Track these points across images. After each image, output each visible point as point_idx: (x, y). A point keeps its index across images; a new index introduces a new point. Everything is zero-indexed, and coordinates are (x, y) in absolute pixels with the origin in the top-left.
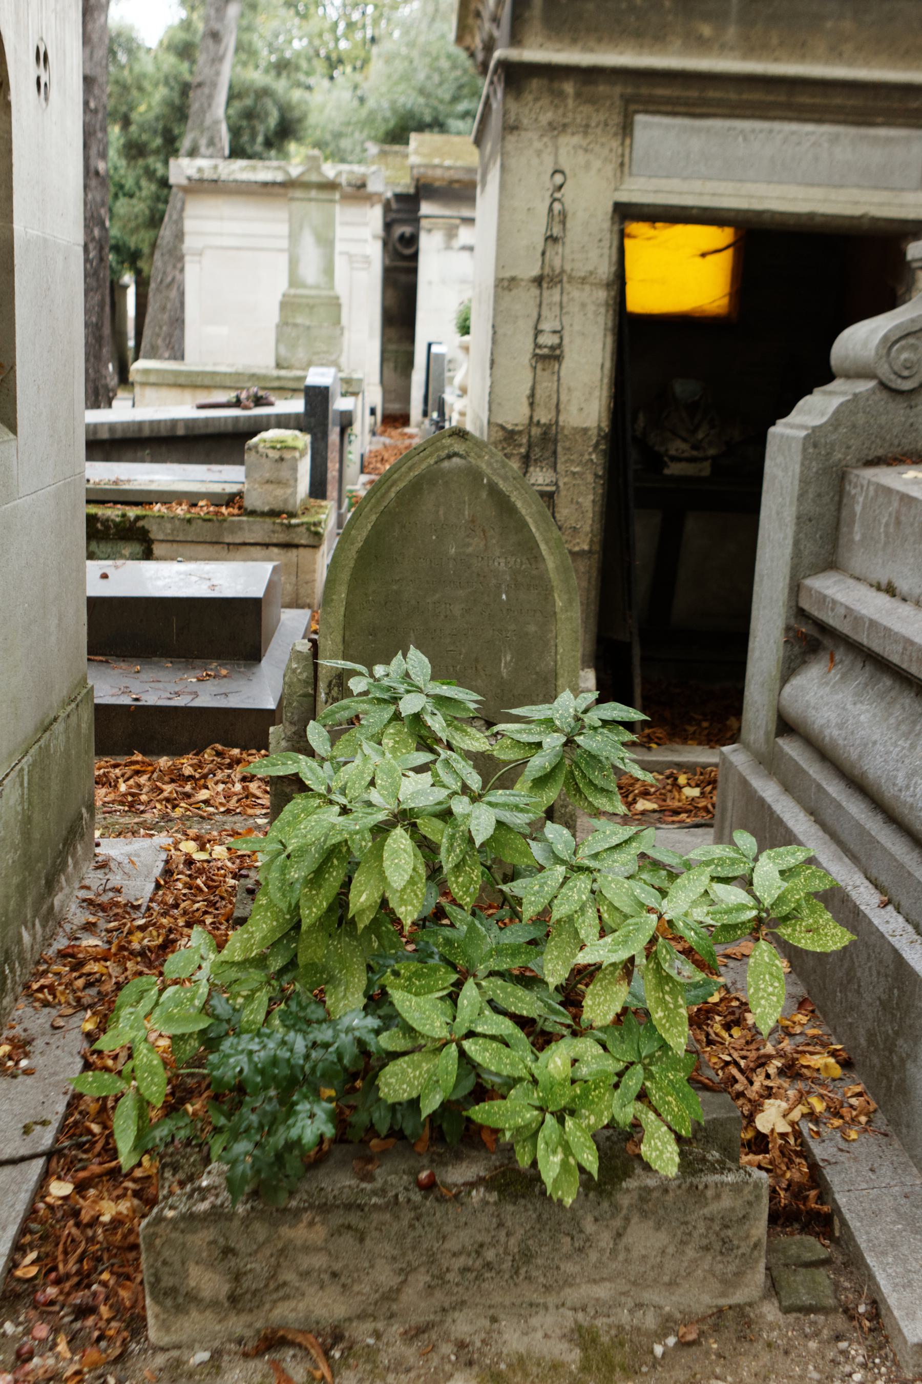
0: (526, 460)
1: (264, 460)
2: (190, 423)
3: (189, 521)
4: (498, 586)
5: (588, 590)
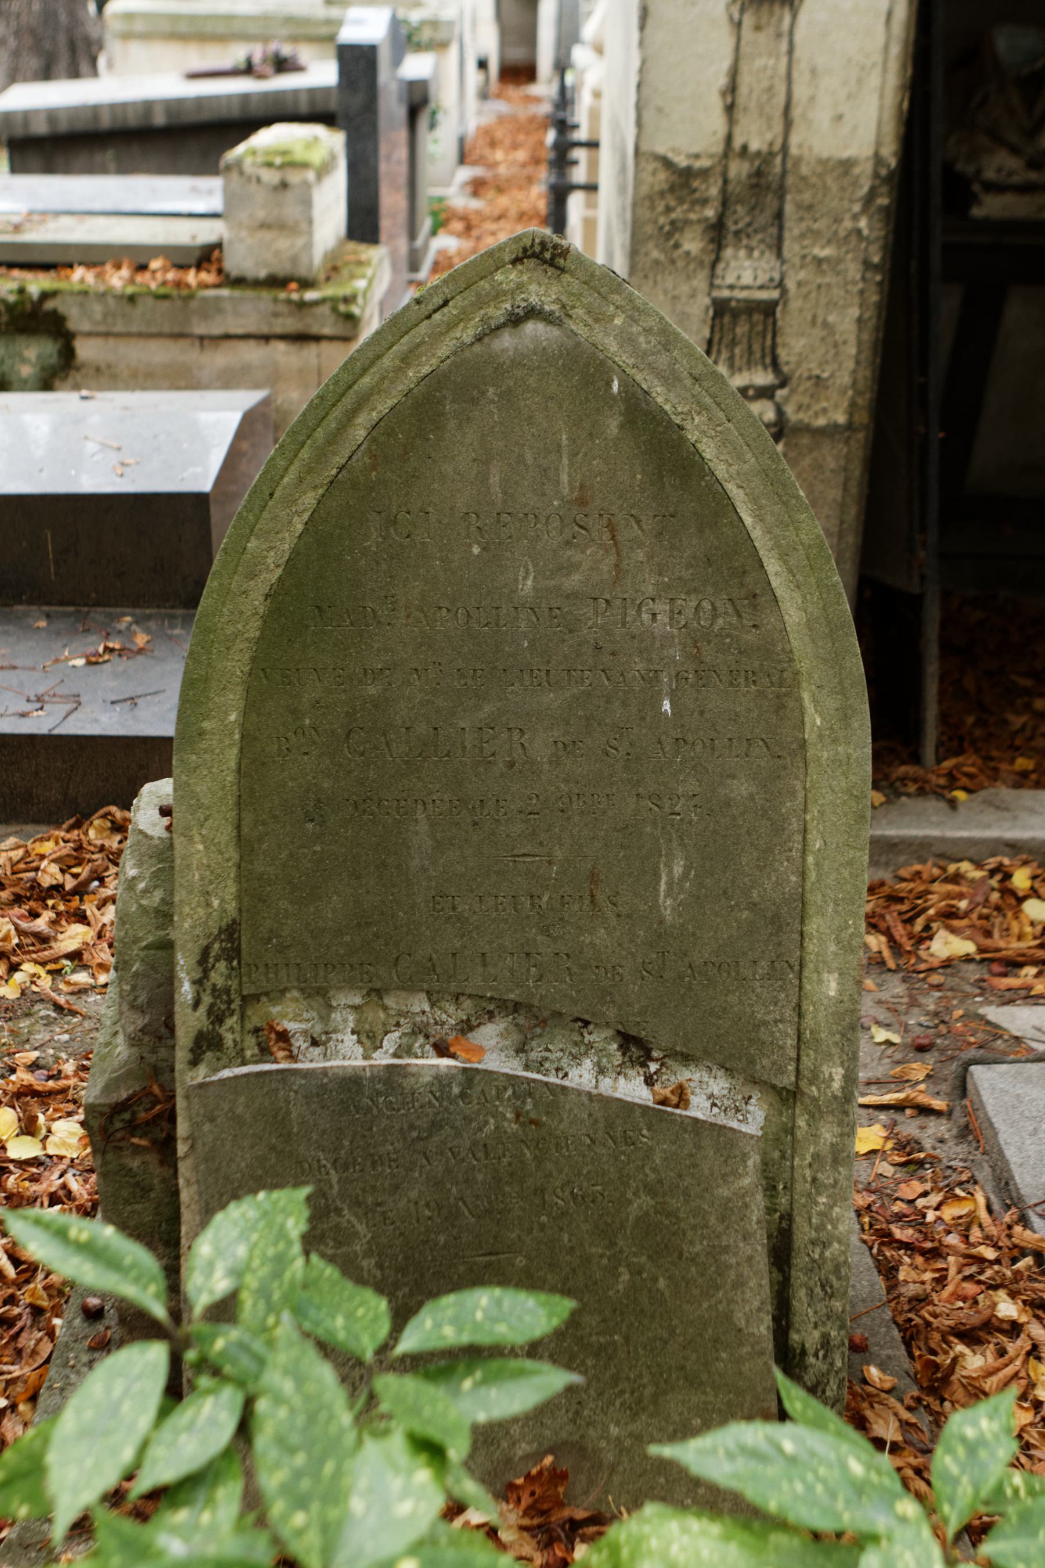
0: (718, 233)
1: (253, 187)
2: (173, 106)
3: (132, 299)
4: (652, 679)
5: (843, 506)
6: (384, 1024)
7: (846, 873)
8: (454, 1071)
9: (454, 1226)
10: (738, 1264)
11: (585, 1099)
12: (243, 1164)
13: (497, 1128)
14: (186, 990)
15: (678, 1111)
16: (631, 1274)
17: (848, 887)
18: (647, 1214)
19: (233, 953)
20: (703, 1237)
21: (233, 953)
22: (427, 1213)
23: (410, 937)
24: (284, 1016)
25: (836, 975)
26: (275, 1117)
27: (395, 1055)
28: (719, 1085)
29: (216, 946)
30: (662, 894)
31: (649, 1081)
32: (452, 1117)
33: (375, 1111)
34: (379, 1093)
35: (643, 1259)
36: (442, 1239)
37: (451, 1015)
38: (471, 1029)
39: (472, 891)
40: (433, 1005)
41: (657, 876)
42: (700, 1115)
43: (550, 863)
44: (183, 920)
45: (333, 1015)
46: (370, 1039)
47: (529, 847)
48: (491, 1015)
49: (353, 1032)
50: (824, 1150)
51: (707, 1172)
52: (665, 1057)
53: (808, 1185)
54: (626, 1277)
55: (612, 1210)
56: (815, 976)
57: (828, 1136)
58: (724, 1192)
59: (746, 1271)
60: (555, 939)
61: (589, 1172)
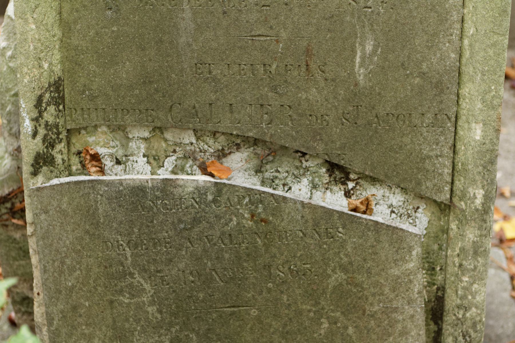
6: (165, 151)
7: (491, 52)
8: (209, 185)
9: (209, 288)
10: (404, 320)
11: (299, 206)
12: (68, 242)
13: (238, 224)
14: (27, 125)
15: (364, 216)
16: (330, 323)
17: (492, 62)
18: (341, 284)
19: (59, 100)
20: (380, 301)
21: (59, 100)
22: (191, 278)
23: (180, 92)
24: (98, 144)
25: (481, 125)
26: (88, 212)
27: (173, 172)
28: (397, 199)
29: (47, 95)
30: (357, 65)
31: (348, 194)
32: (207, 215)
33: (155, 210)
34: (158, 198)
35: (338, 314)
36: (201, 295)
37: (211, 146)
38: (225, 155)
39: (223, 60)
40: (198, 139)
41: (354, 52)
42: (380, 220)
43: (277, 41)
44: (24, 77)
45: (130, 144)
46: (155, 160)
47: (263, 30)
48: (238, 147)
49: (144, 156)
50: (468, 246)
51: (384, 258)
52: (359, 178)
53: (456, 269)
54: (326, 325)
55: (317, 281)
56: (466, 126)
57: (471, 236)
58: (395, 272)
59: (409, 325)
60: (281, 96)
61: (301, 255)
